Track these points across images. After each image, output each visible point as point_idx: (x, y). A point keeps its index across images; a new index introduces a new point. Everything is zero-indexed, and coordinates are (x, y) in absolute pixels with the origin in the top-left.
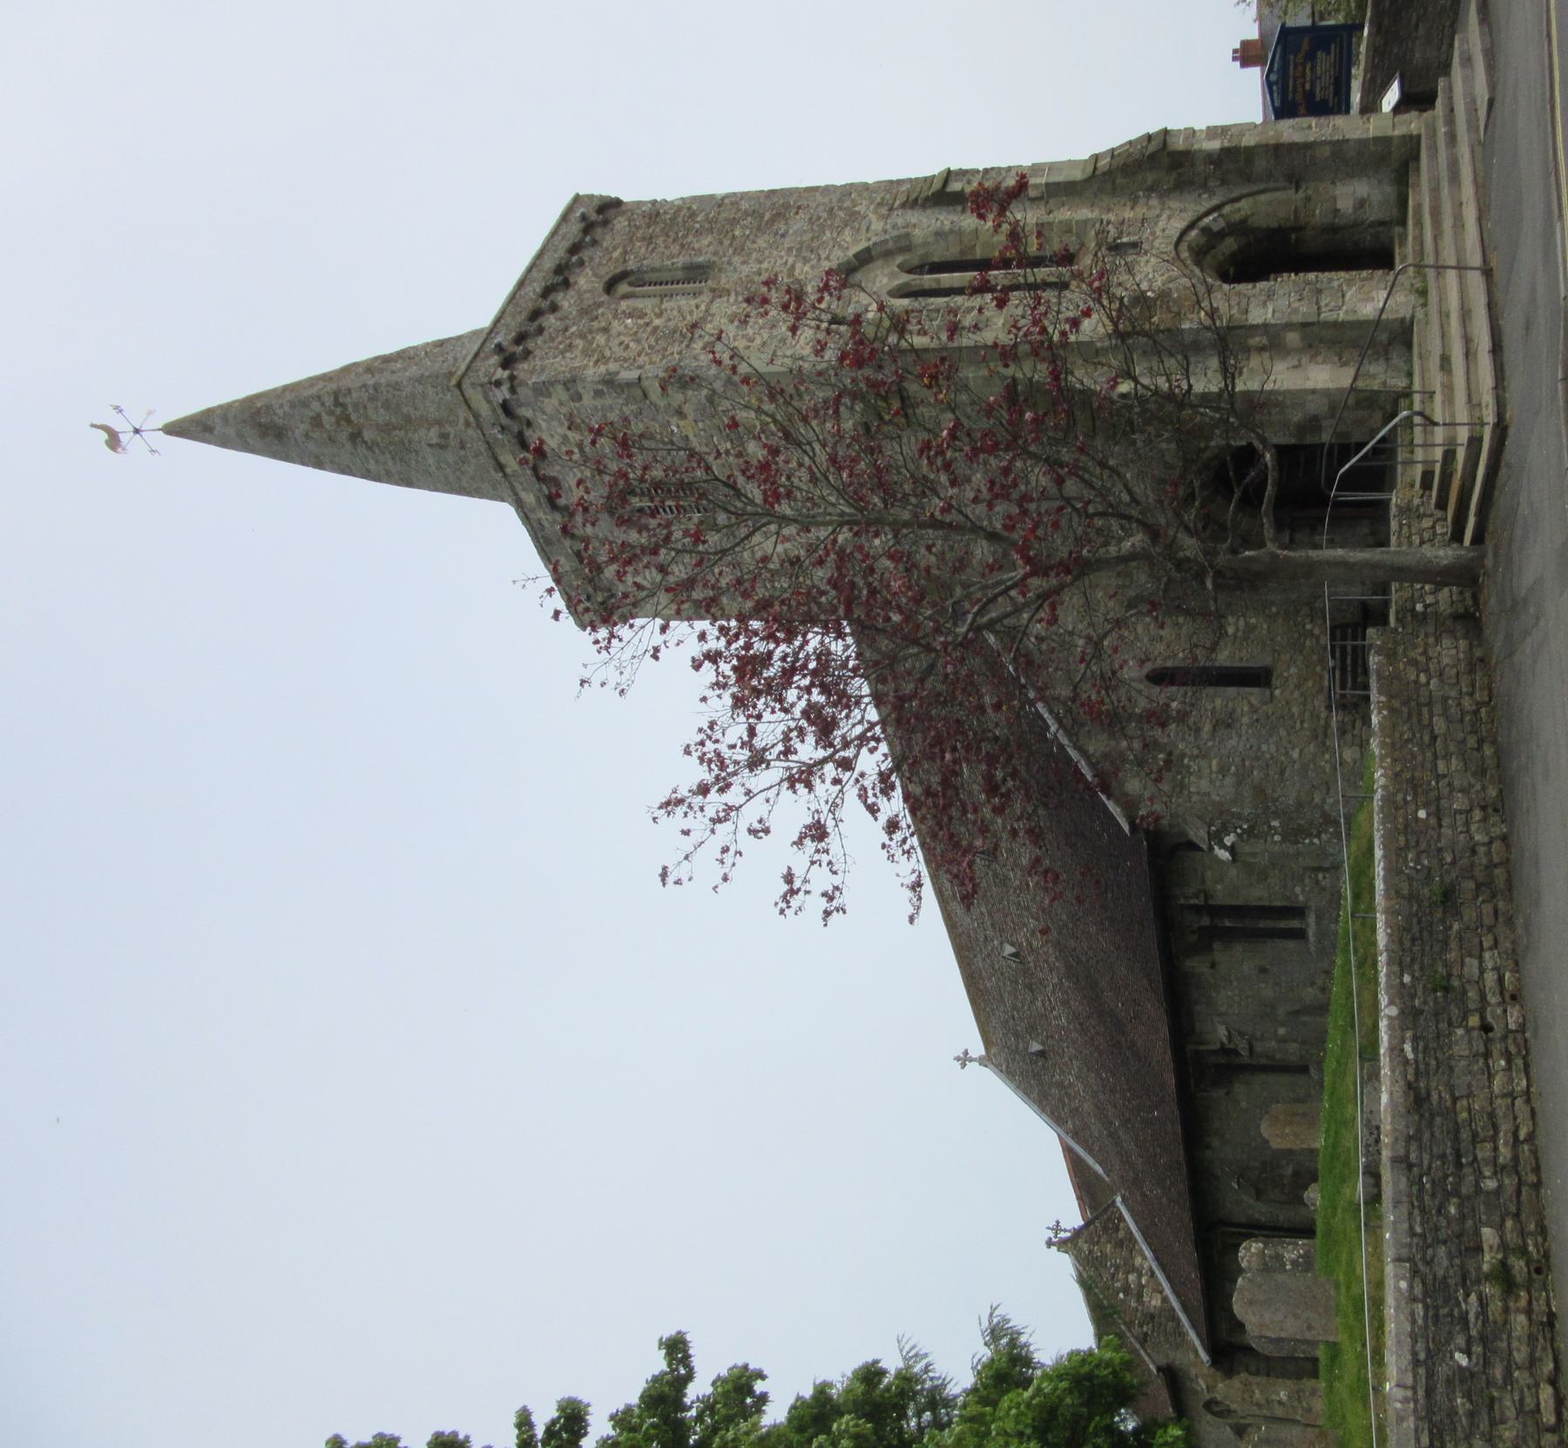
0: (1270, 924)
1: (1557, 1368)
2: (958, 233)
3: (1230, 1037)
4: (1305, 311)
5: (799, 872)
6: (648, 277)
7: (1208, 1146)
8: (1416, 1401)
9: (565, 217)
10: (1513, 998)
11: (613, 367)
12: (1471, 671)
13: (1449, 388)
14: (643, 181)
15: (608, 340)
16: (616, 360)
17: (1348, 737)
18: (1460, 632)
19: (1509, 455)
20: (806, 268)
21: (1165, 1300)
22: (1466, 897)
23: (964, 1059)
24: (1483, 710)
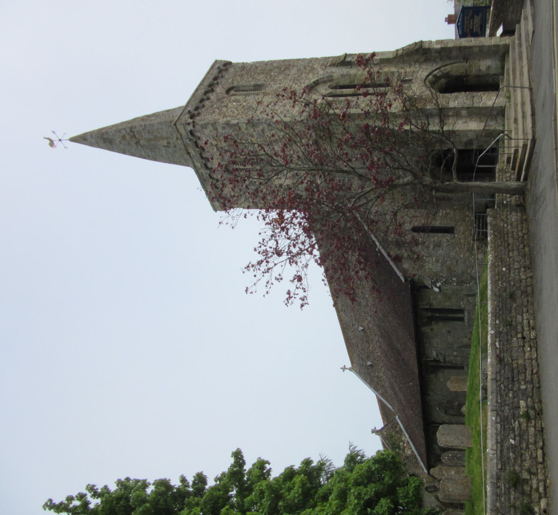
0: (452, 315)
1: (544, 444)
2: (349, 75)
3: (437, 355)
4: (468, 103)
5: (292, 291)
6: (241, 89)
7: (429, 395)
8: (497, 454)
9: (212, 68)
10: (533, 328)
11: (229, 119)
12: (522, 223)
13: (517, 129)
14: (237, 57)
15: (227, 110)
16: (230, 116)
17: (480, 250)
18: (519, 210)
19: (536, 150)
20: (296, 86)
21: (412, 452)
22: (518, 298)
23: (344, 368)
24: (525, 236)
